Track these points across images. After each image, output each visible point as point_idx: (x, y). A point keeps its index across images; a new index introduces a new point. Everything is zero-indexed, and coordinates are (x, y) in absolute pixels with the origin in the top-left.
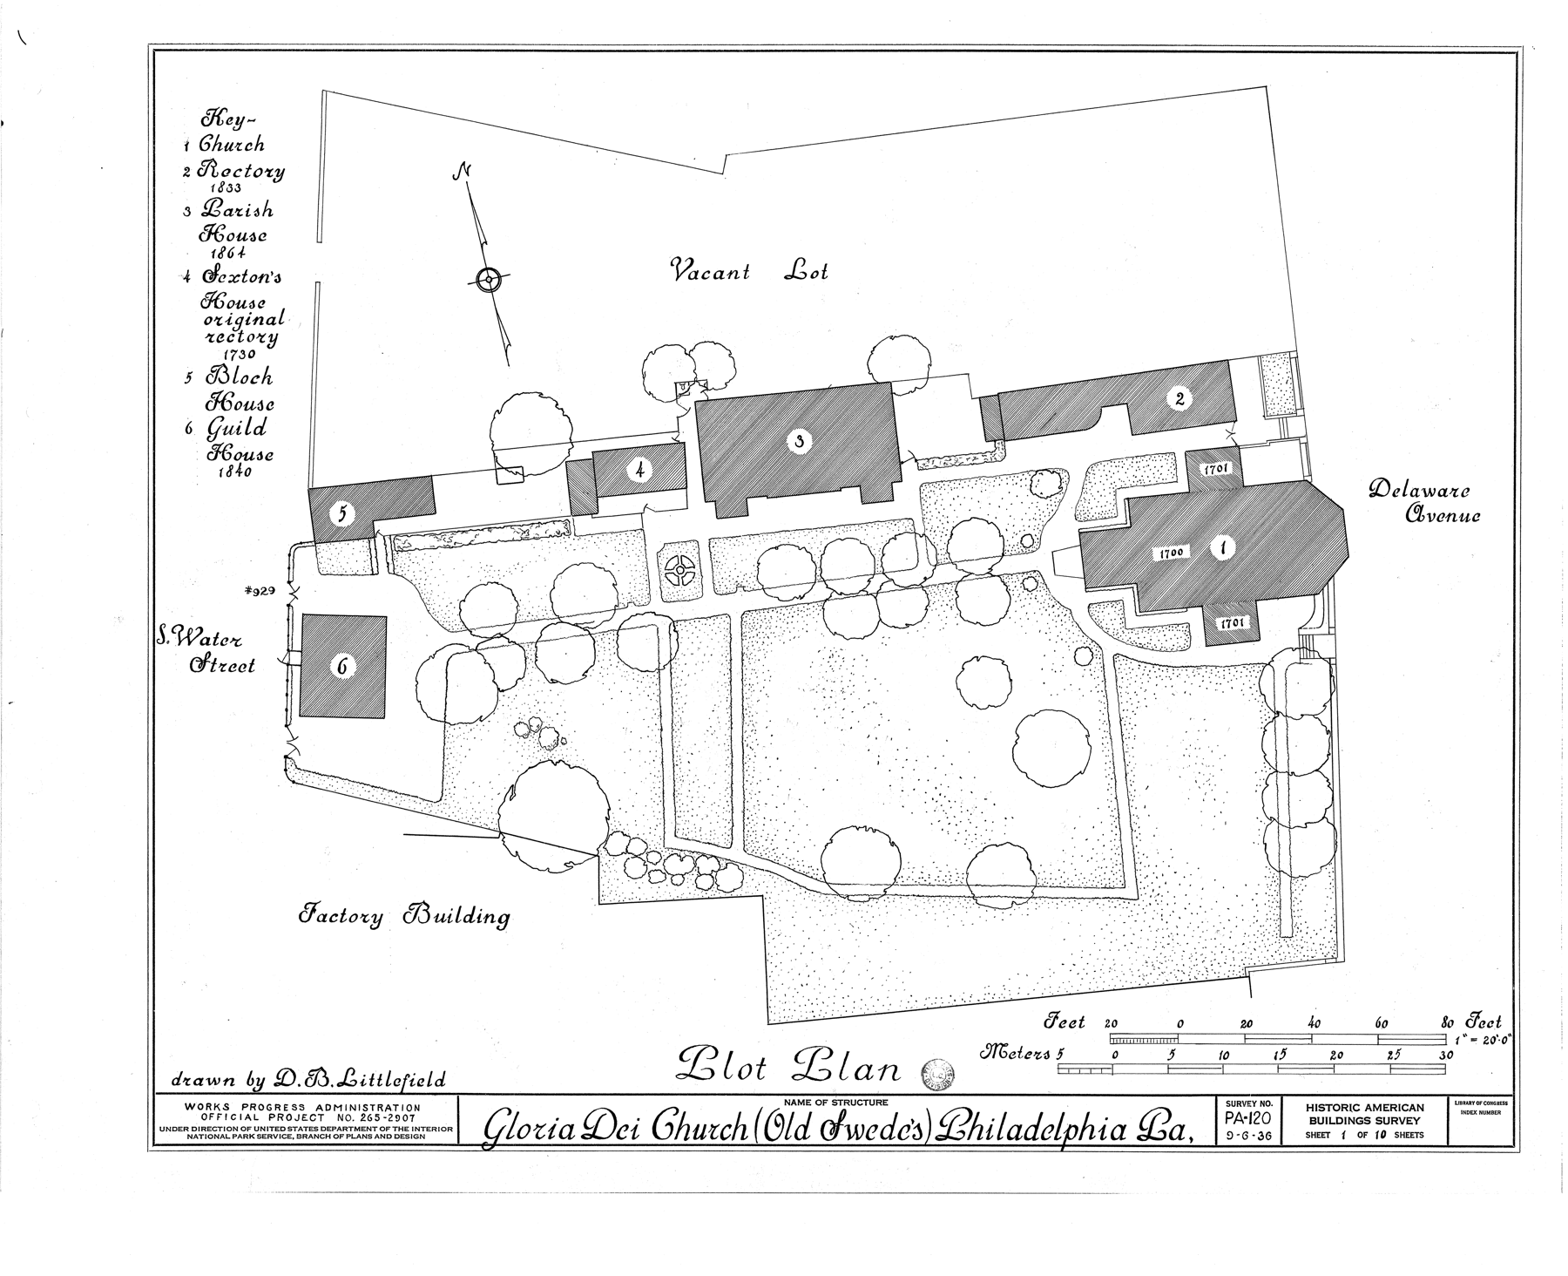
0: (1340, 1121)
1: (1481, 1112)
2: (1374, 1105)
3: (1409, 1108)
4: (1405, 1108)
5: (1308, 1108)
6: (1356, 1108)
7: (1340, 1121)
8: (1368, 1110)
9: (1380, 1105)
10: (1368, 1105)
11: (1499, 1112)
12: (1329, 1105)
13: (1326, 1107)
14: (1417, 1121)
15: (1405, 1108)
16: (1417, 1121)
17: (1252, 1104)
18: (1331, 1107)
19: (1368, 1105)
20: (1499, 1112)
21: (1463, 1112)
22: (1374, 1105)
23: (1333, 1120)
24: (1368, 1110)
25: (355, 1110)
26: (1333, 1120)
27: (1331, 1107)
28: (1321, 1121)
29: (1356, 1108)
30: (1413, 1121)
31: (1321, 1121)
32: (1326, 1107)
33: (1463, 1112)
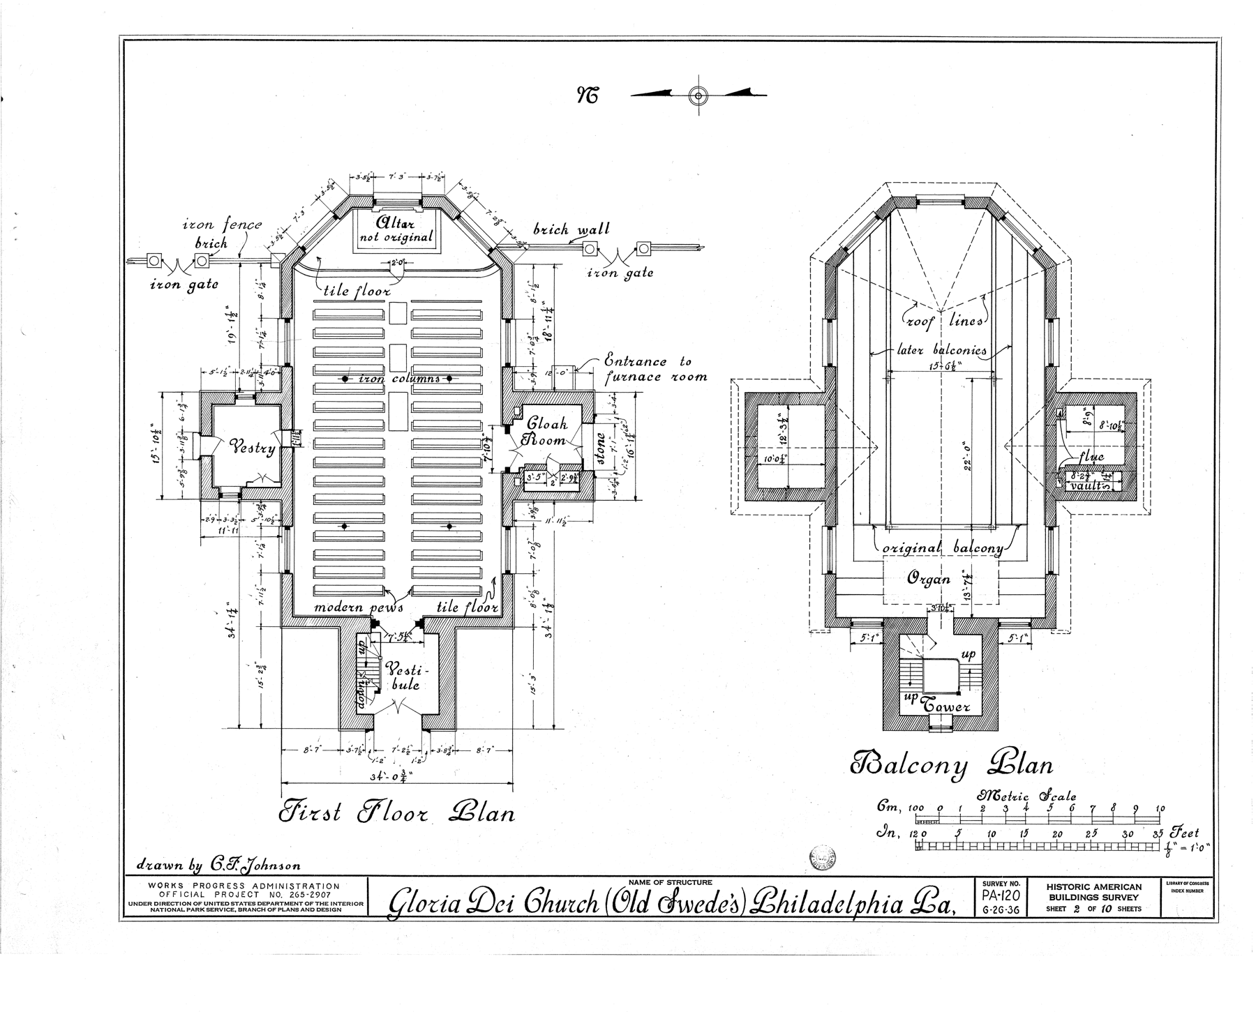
0: (1074, 897)
2: (1101, 885)
3: (1129, 887)
4: (1126, 887)
5: (1048, 887)
6: (1087, 887)
8: (1097, 889)
9: (1106, 885)
10: (1097, 885)
11: (1202, 891)
12: (1065, 885)
13: (1063, 887)
14: (1136, 898)
15: (1126, 887)
16: (1136, 898)
17: (1003, 884)
18: (1067, 887)
19: (1097, 885)
20: (1202, 891)
21: (1173, 891)
22: (1101, 885)
23: (1069, 897)
24: (1097, 889)
25: (1082, 896)
26: (1069, 897)
27: (1067, 887)
28: (1058, 898)
29: (1087, 887)
30: (1133, 898)
31: (1058, 898)
32: (1063, 887)
33: (1173, 891)
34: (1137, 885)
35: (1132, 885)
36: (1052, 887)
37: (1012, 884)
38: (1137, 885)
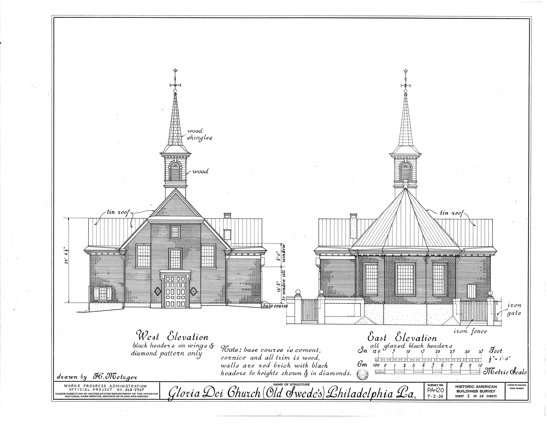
0: (467, 391)
1: (517, 388)
3: (491, 387)
4: (490, 387)
5: (456, 387)
6: (473, 387)
7: (467, 391)
8: (477, 388)
9: (481, 386)
10: (477, 386)
11: (523, 388)
13: (463, 387)
14: (494, 391)
15: (490, 387)
16: (494, 391)
17: (436, 385)
19: (477, 386)
20: (523, 388)
21: (511, 388)
23: (465, 391)
25: (471, 390)
26: (465, 391)
27: (464, 386)
29: (473, 387)
30: (493, 391)
31: (461, 391)
32: (463, 387)
33: (511, 388)
34: (495, 386)
35: (493, 386)
36: (458, 387)
37: (440, 385)
38: (495, 386)
